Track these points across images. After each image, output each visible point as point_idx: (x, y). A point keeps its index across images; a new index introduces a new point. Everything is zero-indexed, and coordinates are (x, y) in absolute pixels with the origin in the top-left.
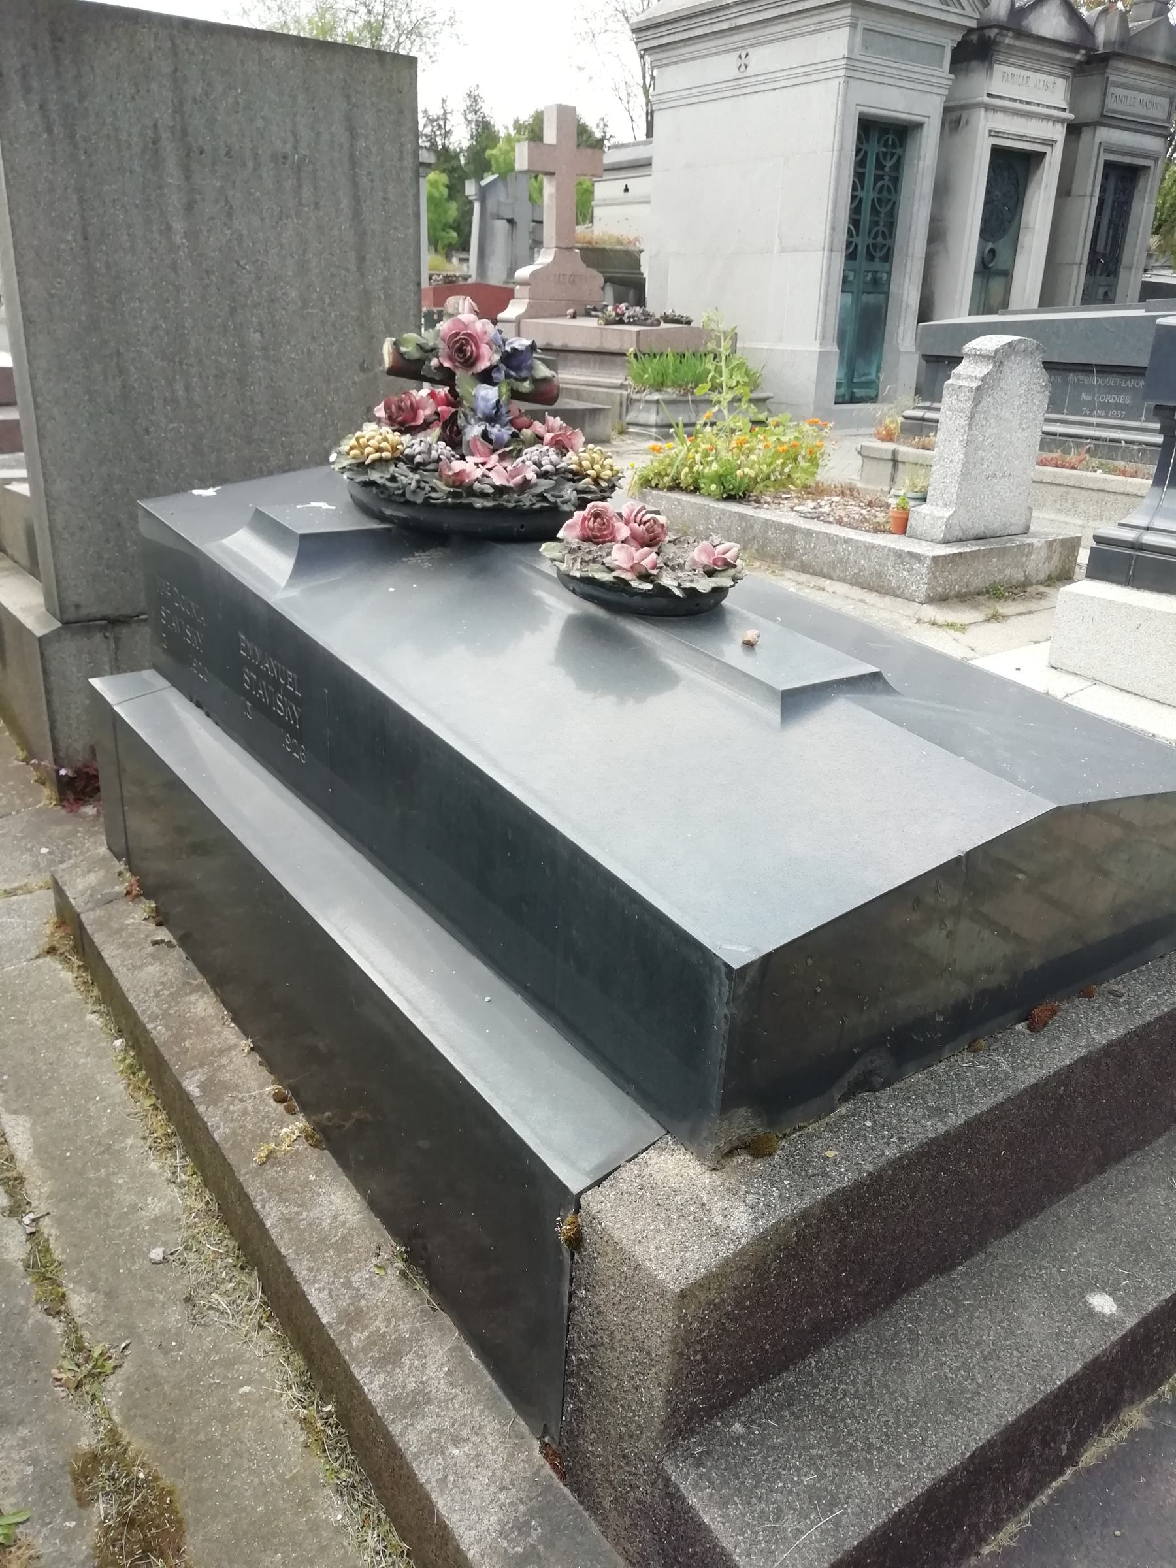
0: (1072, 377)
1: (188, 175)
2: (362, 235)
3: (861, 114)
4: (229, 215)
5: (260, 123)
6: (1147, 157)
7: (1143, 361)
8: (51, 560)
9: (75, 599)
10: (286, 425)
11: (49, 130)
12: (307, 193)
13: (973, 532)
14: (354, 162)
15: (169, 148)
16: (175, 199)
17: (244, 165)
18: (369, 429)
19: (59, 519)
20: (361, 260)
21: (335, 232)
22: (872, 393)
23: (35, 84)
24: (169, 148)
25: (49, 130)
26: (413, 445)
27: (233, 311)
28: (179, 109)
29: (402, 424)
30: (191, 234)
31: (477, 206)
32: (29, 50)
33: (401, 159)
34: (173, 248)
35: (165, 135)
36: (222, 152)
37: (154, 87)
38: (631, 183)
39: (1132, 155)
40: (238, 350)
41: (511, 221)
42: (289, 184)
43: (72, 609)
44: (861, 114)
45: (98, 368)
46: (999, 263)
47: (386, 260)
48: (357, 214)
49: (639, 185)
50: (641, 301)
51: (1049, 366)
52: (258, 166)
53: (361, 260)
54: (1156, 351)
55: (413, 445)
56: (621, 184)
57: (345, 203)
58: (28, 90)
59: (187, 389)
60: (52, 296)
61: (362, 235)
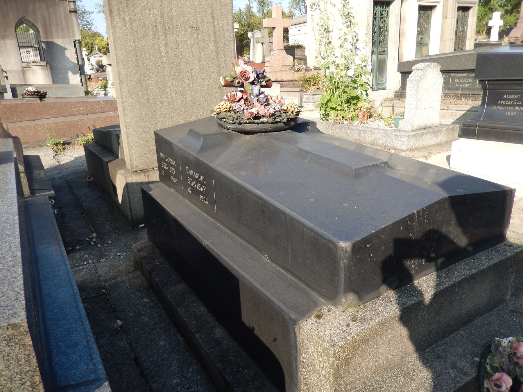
0: (451, 75)
1: (165, 34)
2: (217, 48)
3: (515, 190)
4: (178, 46)
5: (186, 18)
6: (472, 4)
7: (474, 67)
8: (128, 153)
9: (135, 164)
10: (197, 107)
11: (126, 26)
12: (200, 37)
13: (421, 127)
14: (214, 27)
15: (159, 27)
16: (162, 42)
17: (182, 31)
18: (222, 103)
19: (130, 140)
20: (218, 55)
21: (209, 48)
22: (384, 87)
23: (121, 13)
24: (159, 27)
25: (126, 26)
26: (235, 106)
27: (179, 74)
28: (162, 16)
29: (232, 101)
30: (167, 52)
31: (252, 40)
32: (120, 4)
33: (228, 24)
34: (161, 57)
35: (159, 24)
36: (175, 28)
37: (155, 11)
38: (300, 28)
39: (467, 3)
40: (181, 85)
41: (262, 43)
42: (195, 35)
43: (135, 167)
44: (515, 190)
45: (141, 94)
46: (424, 41)
47: (225, 55)
48: (216, 42)
49: (302, 27)
50: (306, 64)
51: (442, 71)
52: (186, 30)
53: (218, 55)
54: (478, 63)
55: (235, 106)
56: (297, 29)
57: (212, 39)
58: (120, 15)
59: (167, 98)
60: (127, 74)
61: (217, 48)
